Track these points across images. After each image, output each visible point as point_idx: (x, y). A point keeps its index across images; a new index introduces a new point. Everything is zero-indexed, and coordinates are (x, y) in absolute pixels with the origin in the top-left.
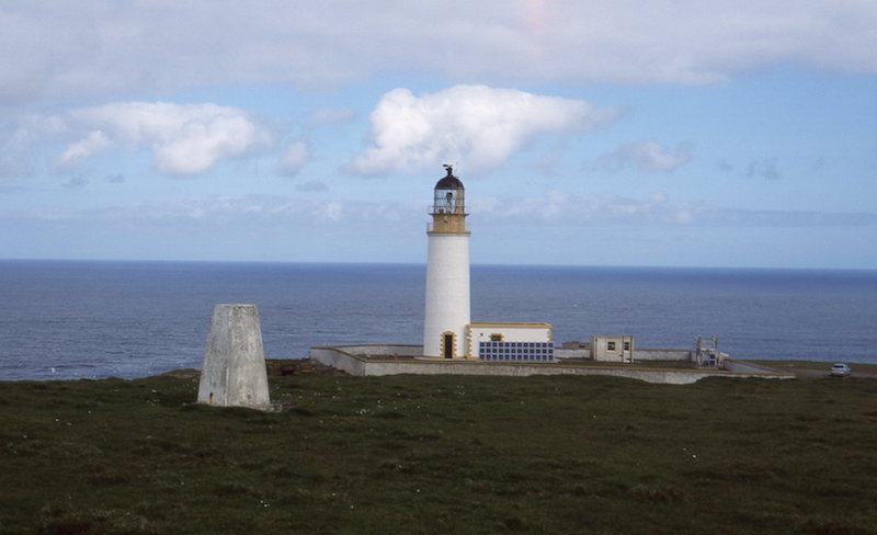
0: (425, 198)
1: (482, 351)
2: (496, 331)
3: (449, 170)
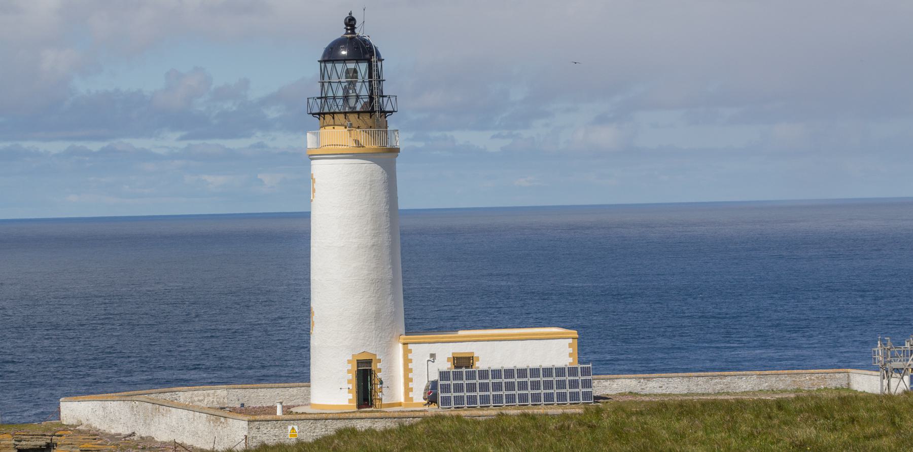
0: (303, 71)
2: (463, 349)
3: (350, 23)
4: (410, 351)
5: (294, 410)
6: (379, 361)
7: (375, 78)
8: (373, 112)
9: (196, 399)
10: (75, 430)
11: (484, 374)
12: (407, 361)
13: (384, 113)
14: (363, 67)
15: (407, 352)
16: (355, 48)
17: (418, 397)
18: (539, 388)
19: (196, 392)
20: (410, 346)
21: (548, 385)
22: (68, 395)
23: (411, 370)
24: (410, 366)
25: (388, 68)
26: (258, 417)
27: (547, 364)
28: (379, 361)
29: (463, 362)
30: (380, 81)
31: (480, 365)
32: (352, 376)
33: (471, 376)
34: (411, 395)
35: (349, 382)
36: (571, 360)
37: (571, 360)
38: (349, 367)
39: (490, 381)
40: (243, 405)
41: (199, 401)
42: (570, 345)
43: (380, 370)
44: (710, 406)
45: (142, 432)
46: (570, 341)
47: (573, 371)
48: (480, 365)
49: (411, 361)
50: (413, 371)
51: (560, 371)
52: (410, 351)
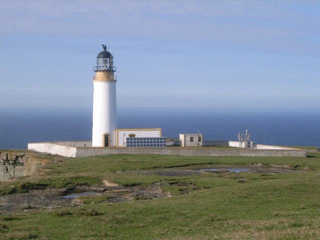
3: (105, 48)
7: (111, 63)
8: (109, 72)
10: (30, 151)
11: (138, 139)
13: (113, 71)
14: (108, 59)
16: (106, 55)
21: (151, 142)
22: (259, 144)
25: (114, 60)
26: (199, 158)
27: (151, 137)
30: (112, 63)
31: (136, 137)
33: (135, 139)
44: (275, 150)
45: (48, 152)
47: (161, 139)
48: (136, 137)
50: (121, 138)
51: (158, 139)
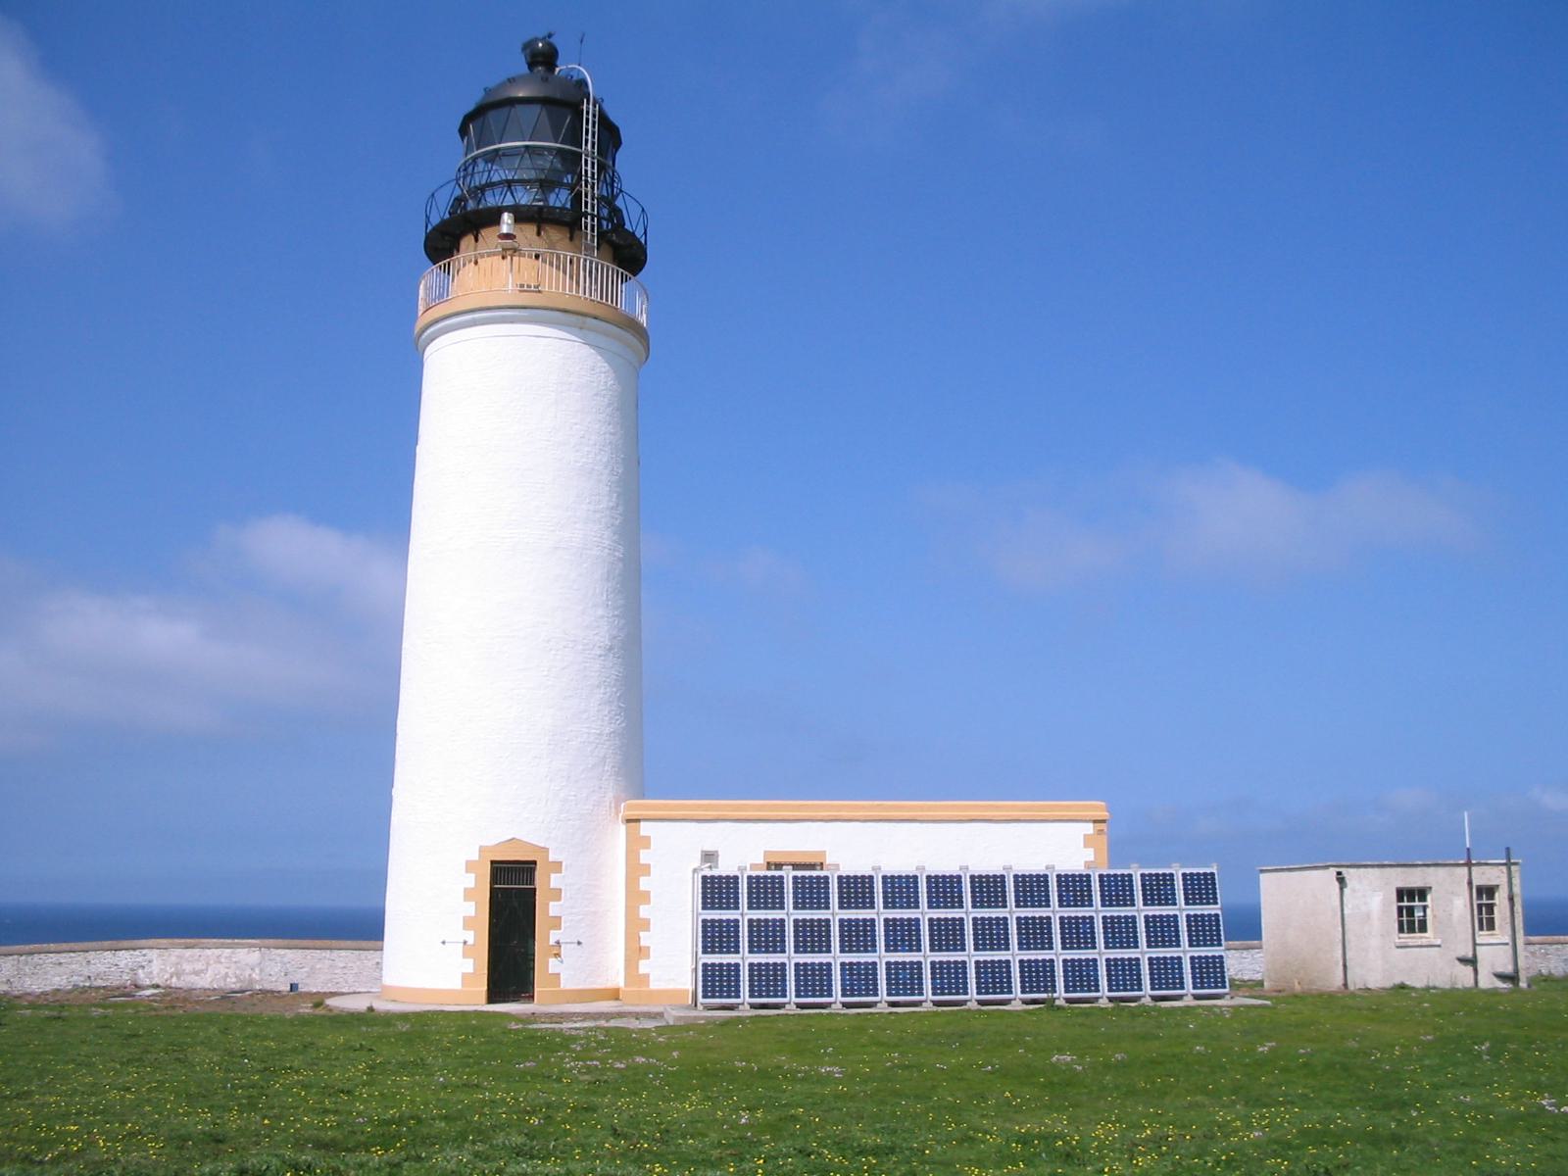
1: (716, 936)
3: (543, 58)
4: (646, 842)
5: (331, 1002)
6: (557, 867)
9: (187, 967)
12: (636, 870)
15: (636, 844)
17: (673, 967)
18: (1408, 916)
19: (188, 952)
20: (645, 828)
23: (645, 897)
24: (644, 911)
28: (557, 867)
29: (607, 1021)
32: (478, 909)
34: (644, 967)
35: (468, 923)
36: (1089, 855)
37: (1089, 855)
38: (470, 881)
39: (879, 914)
40: (293, 987)
41: (197, 973)
42: (1088, 841)
43: (557, 894)
46: (1089, 828)
49: (645, 897)
52: (646, 842)
